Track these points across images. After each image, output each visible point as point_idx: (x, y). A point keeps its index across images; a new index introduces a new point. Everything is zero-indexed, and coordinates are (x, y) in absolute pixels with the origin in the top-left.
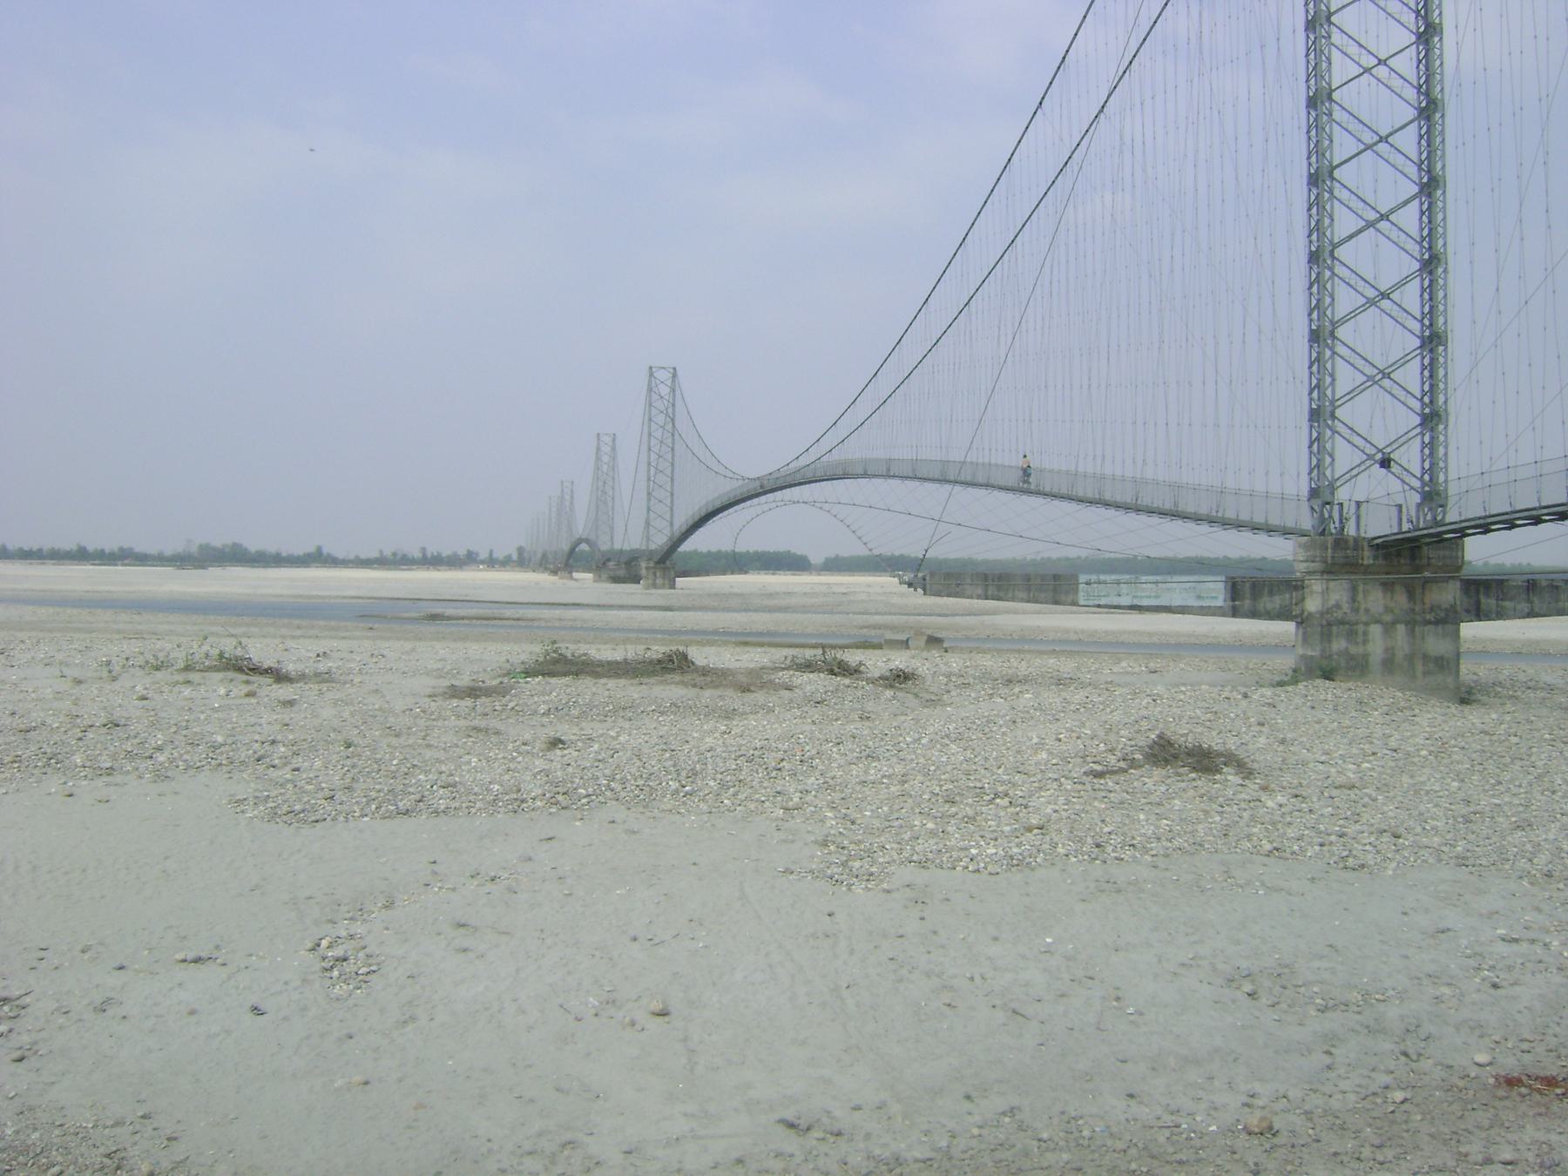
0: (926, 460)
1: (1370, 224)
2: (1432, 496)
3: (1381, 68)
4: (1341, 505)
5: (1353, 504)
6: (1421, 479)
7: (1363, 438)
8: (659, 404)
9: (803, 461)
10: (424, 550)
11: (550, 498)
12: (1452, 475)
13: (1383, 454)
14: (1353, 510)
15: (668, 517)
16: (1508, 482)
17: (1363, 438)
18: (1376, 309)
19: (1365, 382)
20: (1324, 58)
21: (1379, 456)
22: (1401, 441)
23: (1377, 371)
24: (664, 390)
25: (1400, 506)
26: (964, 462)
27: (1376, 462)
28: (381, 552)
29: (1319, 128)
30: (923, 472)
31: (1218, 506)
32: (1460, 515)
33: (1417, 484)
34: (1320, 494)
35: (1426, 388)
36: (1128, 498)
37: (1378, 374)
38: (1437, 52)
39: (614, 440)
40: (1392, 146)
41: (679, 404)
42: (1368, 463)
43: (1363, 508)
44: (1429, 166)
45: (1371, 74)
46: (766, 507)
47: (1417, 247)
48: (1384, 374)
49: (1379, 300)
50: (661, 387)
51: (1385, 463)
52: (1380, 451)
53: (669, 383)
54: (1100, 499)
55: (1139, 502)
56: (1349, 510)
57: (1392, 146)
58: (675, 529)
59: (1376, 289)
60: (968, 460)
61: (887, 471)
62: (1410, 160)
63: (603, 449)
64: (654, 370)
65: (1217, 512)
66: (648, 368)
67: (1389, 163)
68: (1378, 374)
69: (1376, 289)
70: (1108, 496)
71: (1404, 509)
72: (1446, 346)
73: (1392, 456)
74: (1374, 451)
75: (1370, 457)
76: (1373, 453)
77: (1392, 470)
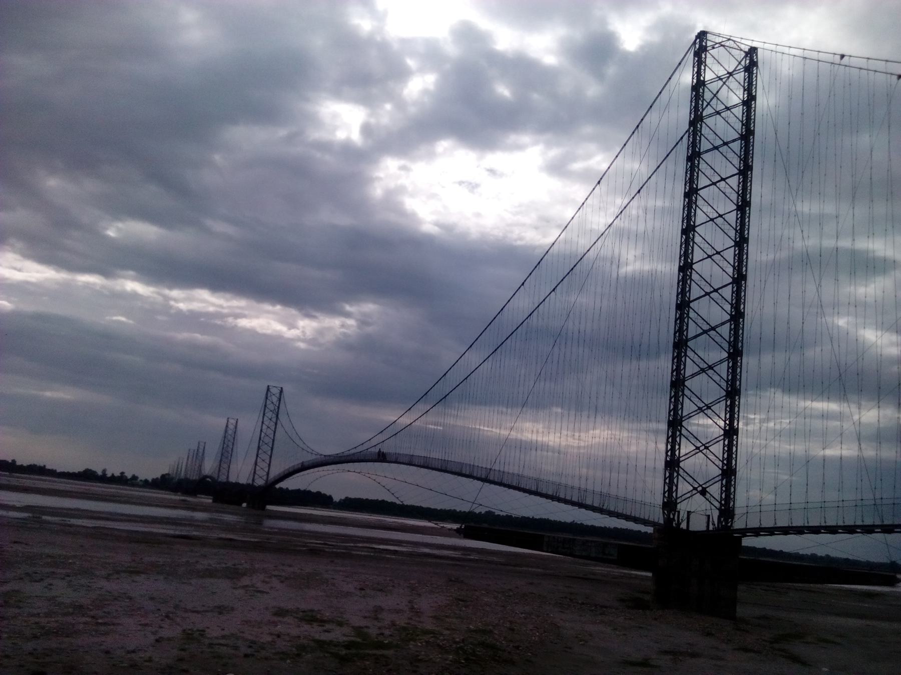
0: (419, 456)
1: (705, 332)
2: (727, 511)
3: (710, 254)
4: (679, 512)
5: (686, 512)
6: (720, 503)
7: (700, 275)
8: (271, 407)
9: (359, 449)
10: (104, 471)
11: (189, 450)
12: (738, 504)
13: (703, 488)
14: (686, 516)
15: (266, 470)
16: (838, 501)
17: (700, 275)
18: (707, 335)
19: (715, 78)
20: (682, 363)
21: (700, 488)
22: (711, 481)
23: (701, 445)
24: (275, 399)
25: (709, 516)
26: (490, 469)
27: (698, 492)
28: (104, 471)
29: (671, 477)
30: (416, 462)
31: (519, 483)
32: (855, 523)
33: (717, 505)
34: (670, 504)
35: (726, 456)
36: (458, 470)
37: (703, 450)
38: (736, 258)
39: (237, 422)
40: (722, 256)
41: (282, 406)
42: (699, 411)
43: (692, 516)
44: (734, 344)
45: (713, 145)
46: (326, 473)
47: (721, 463)
48: (705, 446)
49: (703, 407)
50: (273, 397)
51: (703, 492)
52: (700, 486)
53: (278, 395)
54: (501, 482)
55: (520, 486)
56: (683, 515)
57: (722, 256)
58: (269, 479)
59: (713, 260)
60: (493, 468)
61: (410, 462)
62: (728, 302)
63: (229, 426)
64: (270, 387)
65: (603, 506)
66: (267, 386)
67: (732, 164)
68: (703, 450)
69: (713, 260)
70: (505, 482)
71: (711, 518)
72: (737, 435)
73: (707, 489)
74: (704, 451)
75: (695, 489)
76: (697, 486)
77: (707, 497)
